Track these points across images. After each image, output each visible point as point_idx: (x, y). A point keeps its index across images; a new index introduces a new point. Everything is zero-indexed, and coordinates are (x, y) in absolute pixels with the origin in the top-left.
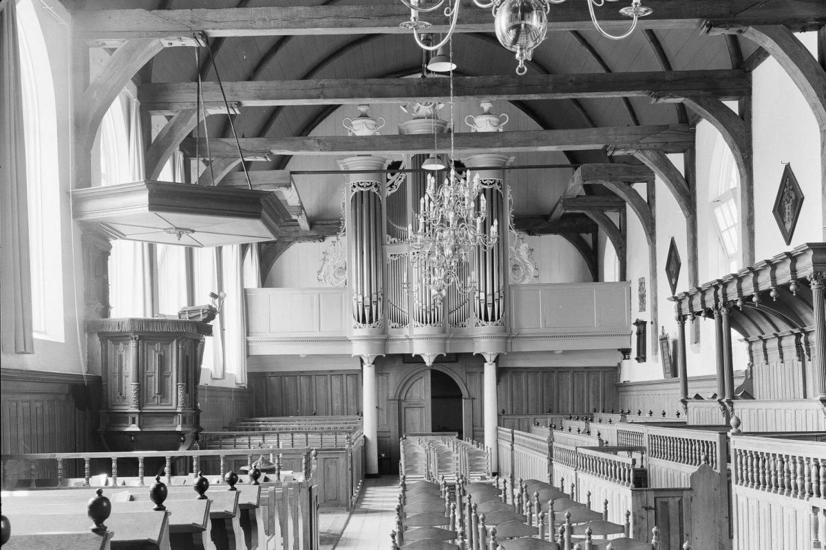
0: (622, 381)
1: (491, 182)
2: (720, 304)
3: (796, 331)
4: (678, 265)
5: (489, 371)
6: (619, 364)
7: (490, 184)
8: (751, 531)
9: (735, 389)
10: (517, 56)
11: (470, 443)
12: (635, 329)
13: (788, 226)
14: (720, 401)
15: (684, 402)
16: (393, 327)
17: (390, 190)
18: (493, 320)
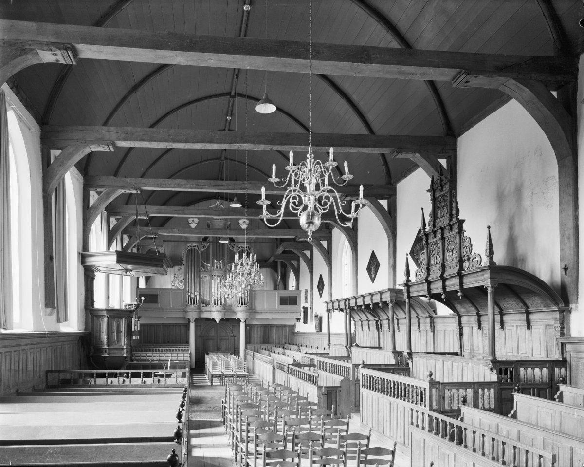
0: (296, 331)
2: (347, 307)
3: (376, 319)
4: (323, 285)
5: (242, 326)
6: (295, 324)
8: (369, 407)
9: (351, 341)
10: (309, 234)
11: (235, 357)
12: (302, 310)
13: (373, 276)
14: (346, 347)
15: (329, 345)
18: (245, 304)
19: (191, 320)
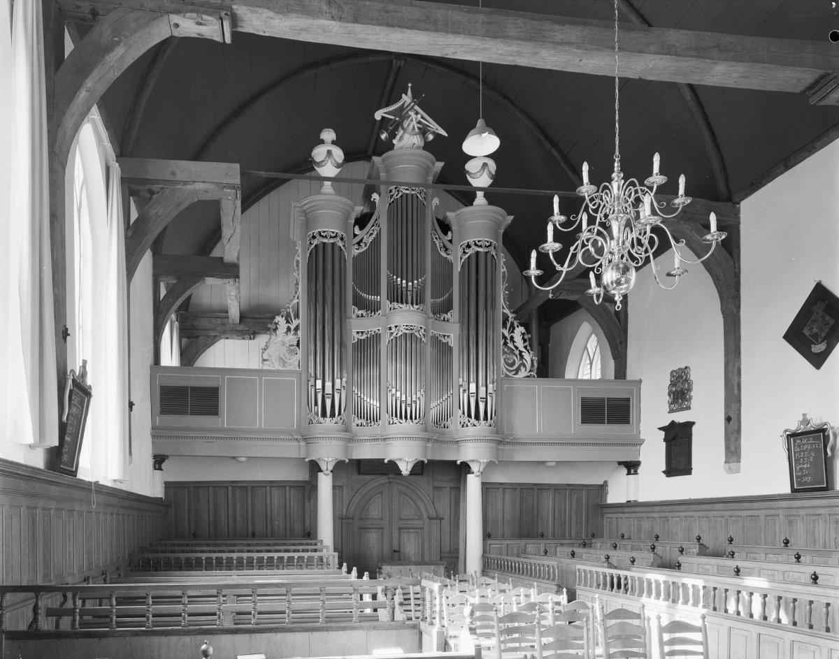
1: (487, 244)
7: (486, 246)
16: (358, 425)
17: (358, 249)
19: (323, 467)
